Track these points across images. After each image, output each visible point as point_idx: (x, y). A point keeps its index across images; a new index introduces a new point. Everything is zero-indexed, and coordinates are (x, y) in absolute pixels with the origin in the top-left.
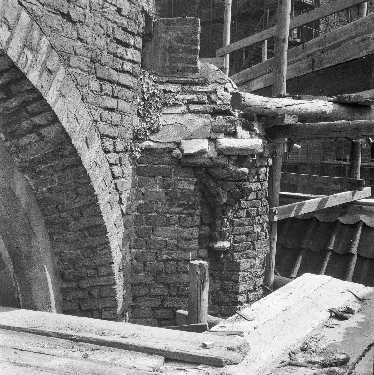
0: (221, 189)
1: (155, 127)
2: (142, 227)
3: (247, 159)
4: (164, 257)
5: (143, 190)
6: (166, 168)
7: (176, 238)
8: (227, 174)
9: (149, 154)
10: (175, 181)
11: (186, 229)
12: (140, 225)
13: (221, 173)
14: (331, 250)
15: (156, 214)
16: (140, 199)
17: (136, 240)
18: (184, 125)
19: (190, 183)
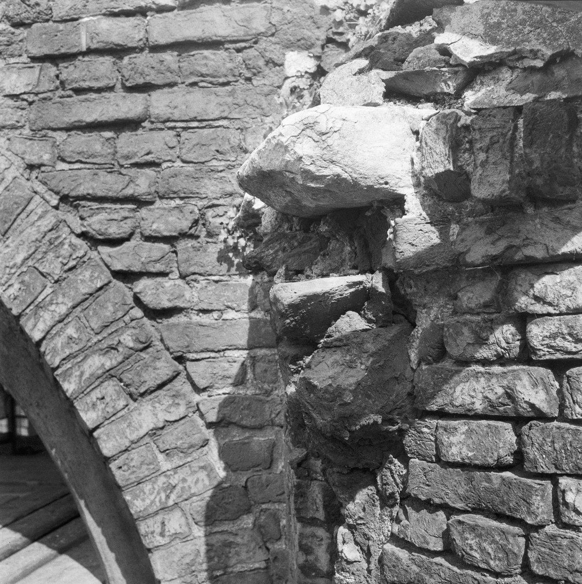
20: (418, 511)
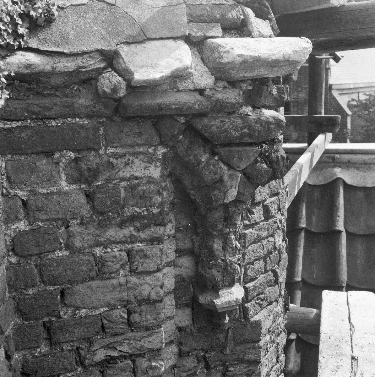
0: (225, 168)
1: (40, 11)
2: (30, 292)
3: (265, 88)
4: (101, 355)
5: (22, 194)
6: (82, 127)
7: (126, 304)
8: (242, 129)
9: (29, 90)
10: (111, 160)
11: (147, 278)
12: (27, 287)
13: (226, 126)
14: (303, 228)
15: (66, 253)
16: (18, 219)
17: (18, 330)
18: (117, 4)
19: (150, 161)
20: (255, 208)
